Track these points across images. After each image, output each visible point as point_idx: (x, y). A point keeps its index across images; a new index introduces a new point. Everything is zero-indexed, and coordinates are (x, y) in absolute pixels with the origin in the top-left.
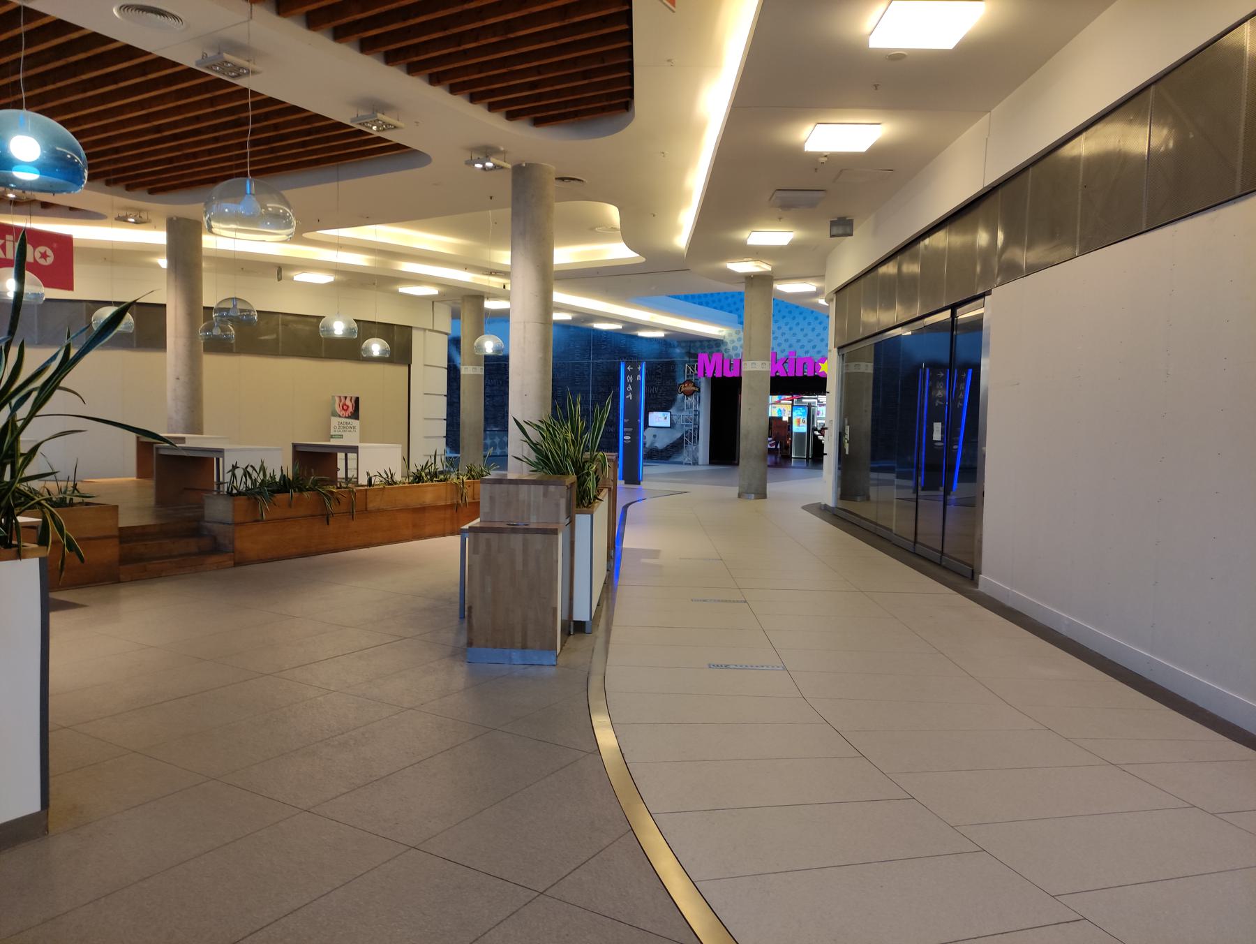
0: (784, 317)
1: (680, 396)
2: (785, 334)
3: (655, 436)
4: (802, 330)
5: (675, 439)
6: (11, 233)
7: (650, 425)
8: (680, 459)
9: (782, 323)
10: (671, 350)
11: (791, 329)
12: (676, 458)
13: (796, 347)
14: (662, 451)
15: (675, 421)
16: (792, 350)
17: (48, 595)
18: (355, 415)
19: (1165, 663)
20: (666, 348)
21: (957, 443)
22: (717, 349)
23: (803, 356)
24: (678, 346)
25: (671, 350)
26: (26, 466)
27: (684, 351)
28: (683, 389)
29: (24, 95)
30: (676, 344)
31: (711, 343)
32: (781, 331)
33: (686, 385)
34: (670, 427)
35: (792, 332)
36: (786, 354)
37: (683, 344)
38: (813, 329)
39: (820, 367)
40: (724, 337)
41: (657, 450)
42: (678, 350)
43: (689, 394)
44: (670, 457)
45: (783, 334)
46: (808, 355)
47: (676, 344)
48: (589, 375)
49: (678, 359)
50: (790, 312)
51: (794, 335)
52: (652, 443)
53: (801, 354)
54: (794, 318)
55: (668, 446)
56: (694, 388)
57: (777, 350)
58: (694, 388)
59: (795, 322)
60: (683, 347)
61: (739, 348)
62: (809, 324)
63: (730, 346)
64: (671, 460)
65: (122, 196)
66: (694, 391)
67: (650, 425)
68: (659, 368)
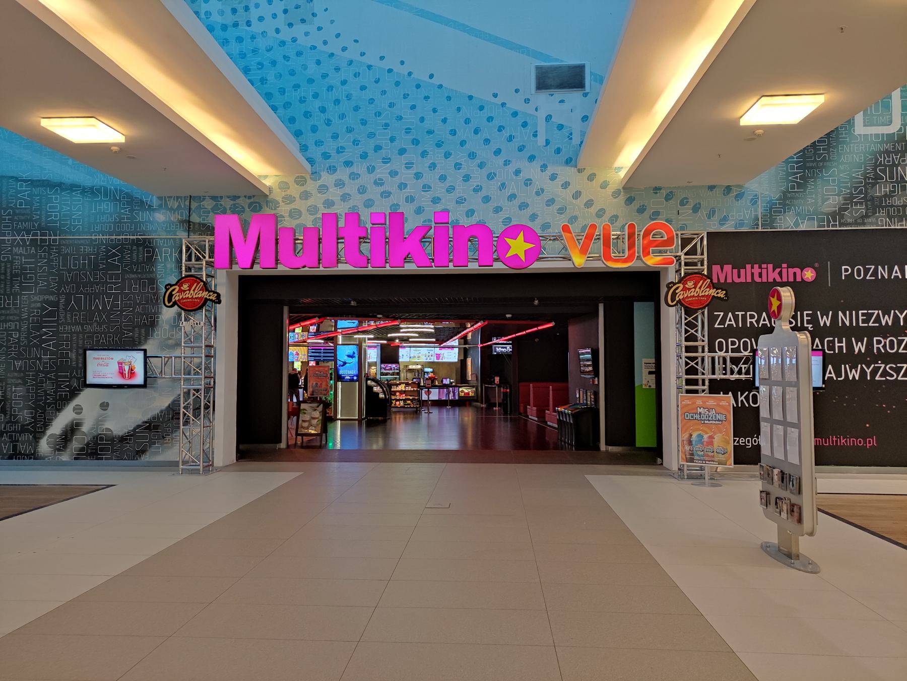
0: (402, 152)
1: (168, 313)
2: (406, 186)
3: (104, 406)
4: (443, 178)
5: (156, 412)
7: (90, 380)
8: (170, 453)
10: (142, 216)
11: (418, 176)
12: (157, 453)
13: (447, 203)
14: (123, 439)
15: (158, 371)
16: (439, 208)
17: (286, 306)
19: (340, 387)
20: (131, 211)
23: (466, 222)
24: (160, 206)
28: (176, 298)
29: (26, 238)
30: (155, 202)
31: (240, 201)
32: (397, 180)
33: (185, 287)
34: (144, 386)
35: (421, 182)
36: (427, 217)
38: (467, 178)
39: (516, 256)
40: (270, 189)
43: (191, 308)
44: (143, 452)
45: (402, 186)
46: (473, 221)
47: (155, 202)
50: (416, 142)
51: (426, 188)
52: (99, 422)
53: (459, 217)
54: (424, 154)
55: (138, 426)
56: (205, 294)
57: (407, 210)
58: (205, 294)
59: (428, 161)
61: (320, 183)
62: (458, 166)
63: (283, 210)
64: (146, 458)
66: (206, 300)
67: (90, 380)
68: (114, 255)
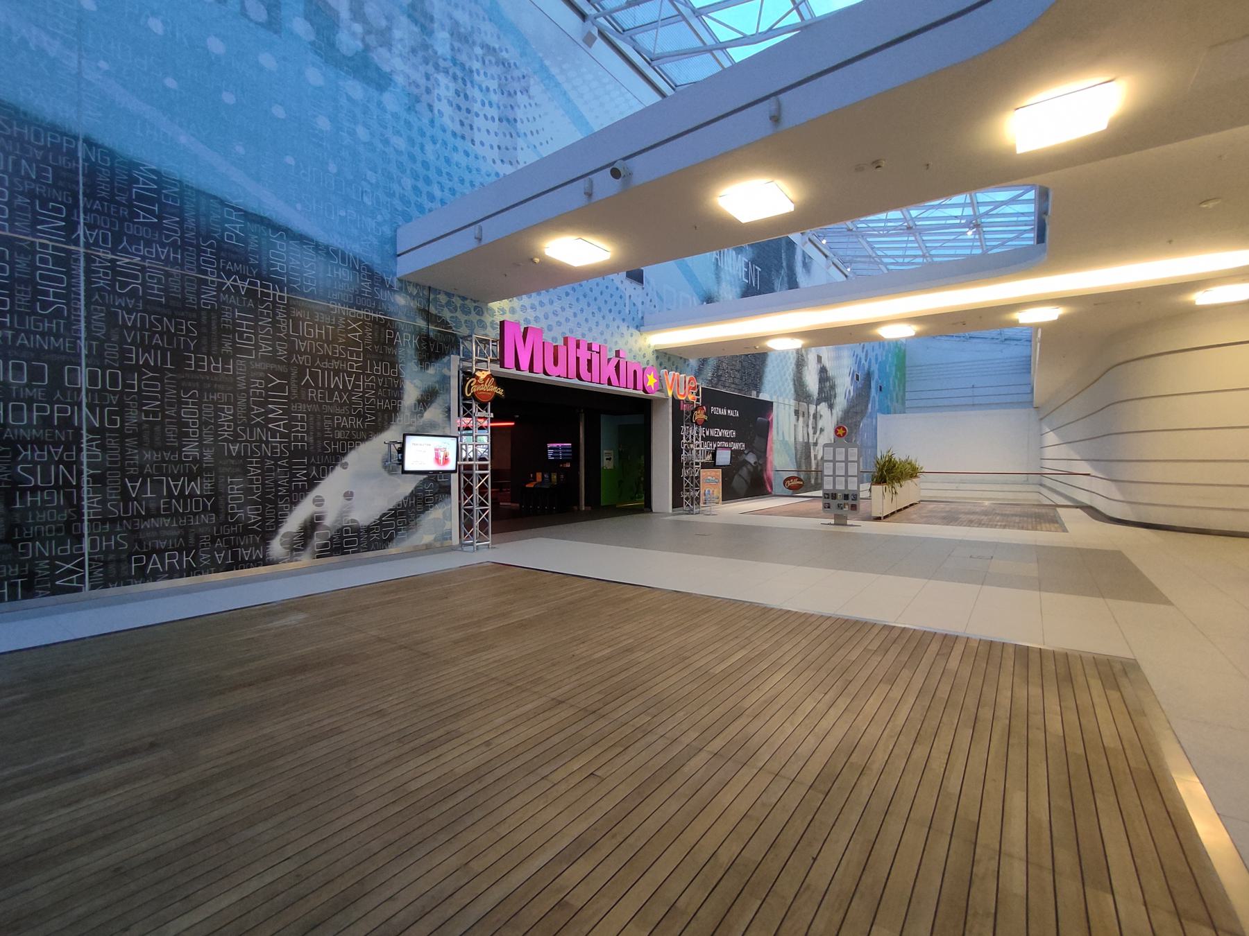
3: (348, 495)
5: (402, 498)
6: (758, 458)
9: (598, 316)
10: (383, 295)
14: (369, 529)
18: (829, 507)
21: (82, 443)
22: (478, 317)
24: (401, 288)
25: (383, 295)
26: (320, 571)
27: (414, 304)
31: (467, 302)
37: (411, 289)
41: (357, 530)
42: (401, 300)
48: (69, 295)
49: (401, 320)
52: (342, 514)
55: (384, 515)
58: (799, 482)
60: (413, 297)
65: (191, 175)
